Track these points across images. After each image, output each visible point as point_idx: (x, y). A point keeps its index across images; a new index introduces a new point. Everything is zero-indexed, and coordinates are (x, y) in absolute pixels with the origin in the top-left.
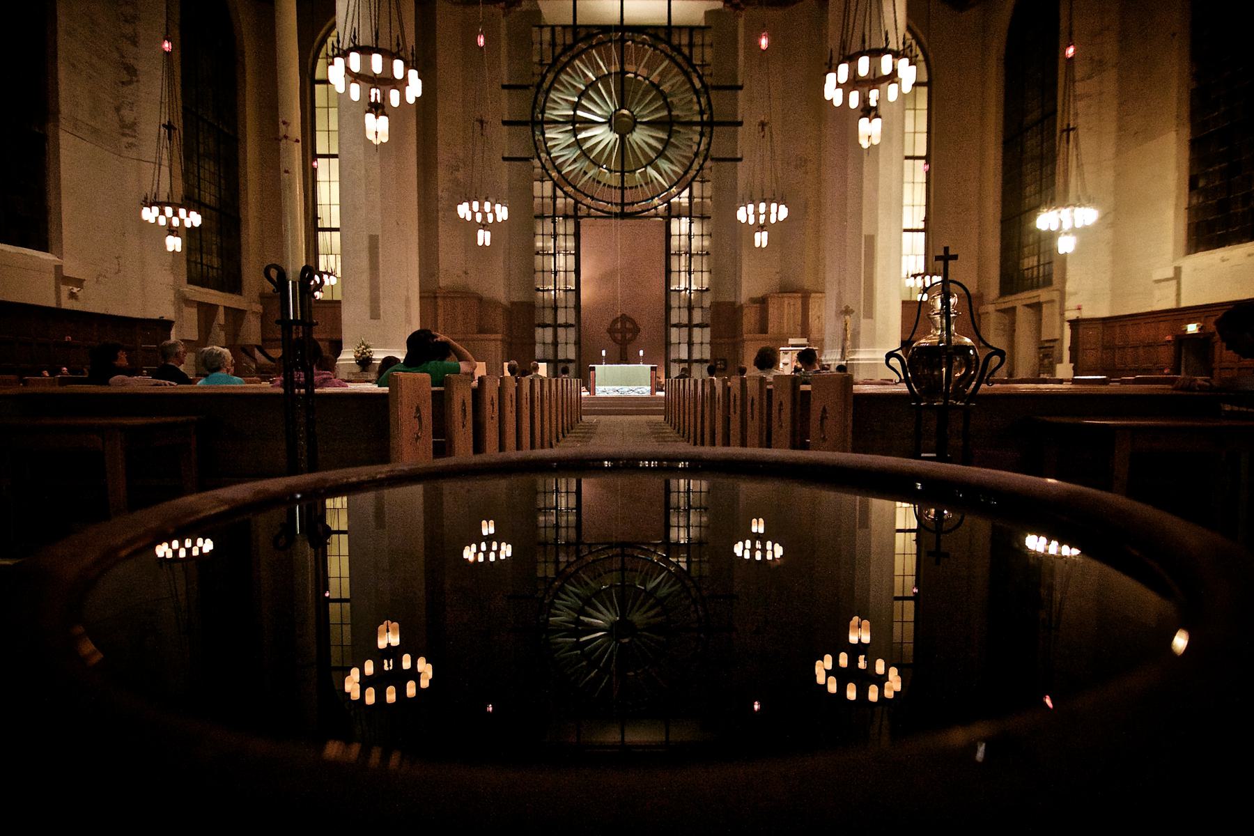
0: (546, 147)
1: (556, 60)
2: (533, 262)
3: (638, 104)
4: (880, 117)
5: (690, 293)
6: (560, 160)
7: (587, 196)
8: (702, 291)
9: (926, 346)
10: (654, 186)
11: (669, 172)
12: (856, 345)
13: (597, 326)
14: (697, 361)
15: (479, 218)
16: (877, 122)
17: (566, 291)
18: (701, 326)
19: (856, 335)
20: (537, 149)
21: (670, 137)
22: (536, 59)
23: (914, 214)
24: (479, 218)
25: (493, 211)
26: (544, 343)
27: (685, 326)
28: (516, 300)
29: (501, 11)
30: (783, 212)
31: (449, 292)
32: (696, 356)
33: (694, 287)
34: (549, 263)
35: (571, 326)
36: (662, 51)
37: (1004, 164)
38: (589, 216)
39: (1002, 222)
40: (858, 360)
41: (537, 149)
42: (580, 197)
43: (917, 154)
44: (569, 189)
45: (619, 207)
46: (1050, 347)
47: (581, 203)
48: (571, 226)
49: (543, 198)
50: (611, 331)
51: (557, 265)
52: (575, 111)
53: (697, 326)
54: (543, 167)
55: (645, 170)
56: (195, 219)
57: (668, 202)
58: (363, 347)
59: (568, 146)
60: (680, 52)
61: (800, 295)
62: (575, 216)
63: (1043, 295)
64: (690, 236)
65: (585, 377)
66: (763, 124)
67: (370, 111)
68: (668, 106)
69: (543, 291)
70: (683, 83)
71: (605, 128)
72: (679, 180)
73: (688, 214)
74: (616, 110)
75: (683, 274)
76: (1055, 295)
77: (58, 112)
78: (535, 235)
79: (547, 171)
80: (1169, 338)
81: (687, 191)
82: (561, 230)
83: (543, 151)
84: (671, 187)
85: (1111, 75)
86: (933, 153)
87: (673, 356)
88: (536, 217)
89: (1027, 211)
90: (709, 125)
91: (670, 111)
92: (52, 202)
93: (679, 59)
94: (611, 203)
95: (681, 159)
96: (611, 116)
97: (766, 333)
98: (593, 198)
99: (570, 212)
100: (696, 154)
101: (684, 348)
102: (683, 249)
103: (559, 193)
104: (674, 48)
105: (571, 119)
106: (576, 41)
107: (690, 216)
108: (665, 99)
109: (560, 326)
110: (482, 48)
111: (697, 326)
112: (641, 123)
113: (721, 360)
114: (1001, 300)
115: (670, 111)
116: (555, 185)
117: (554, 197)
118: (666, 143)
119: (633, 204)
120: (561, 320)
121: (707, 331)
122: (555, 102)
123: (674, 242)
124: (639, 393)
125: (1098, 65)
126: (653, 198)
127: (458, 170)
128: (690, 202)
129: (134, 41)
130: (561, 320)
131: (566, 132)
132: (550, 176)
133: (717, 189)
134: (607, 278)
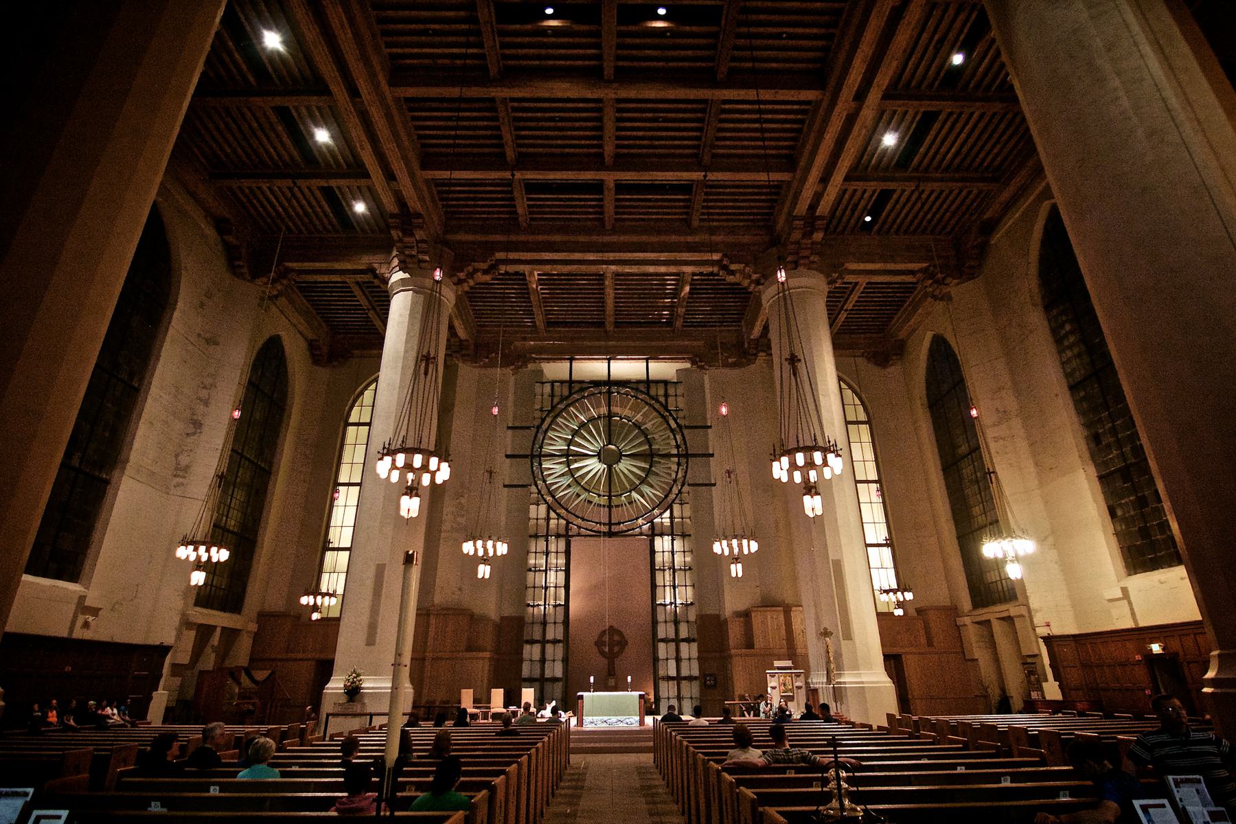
0: (542, 475)
1: (553, 407)
2: (525, 579)
3: (623, 440)
4: (819, 494)
5: (676, 607)
6: (553, 487)
7: (578, 517)
8: (687, 605)
10: (637, 506)
11: (651, 495)
12: (840, 668)
13: (585, 640)
14: (685, 678)
15: (481, 553)
16: (818, 498)
17: (555, 606)
18: (688, 640)
19: (838, 655)
20: (534, 478)
21: (651, 466)
22: (538, 407)
23: (877, 531)
24: (481, 553)
25: (494, 547)
26: (531, 660)
27: (672, 640)
28: (506, 615)
29: (511, 372)
30: (754, 546)
31: (443, 609)
32: (685, 673)
33: (678, 602)
34: (540, 579)
35: (559, 641)
36: (642, 400)
37: (948, 488)
38: (579, 535)
39: (958, 538)
40: (844, 683)
41: (534, 478)
42: (571, 518)
43: (870, 478)
44: (563, 512)
45: (607, 527)
46: (1032, 663)
47: (572, 523)
48: (562, 545)
49: (537, 519)
50: (599, 644)
51: (548, 581)
52: (569, 446)
53: (683, 640)
54: (539, 492)
55: (630, 495)
56: (222, 555)
57: (652, 522)
58: (354, 675)
59: (563, 475)
60: (657, 401)
61: (781, 608)
62: (566, 536)
63: (1013, 610)
64: (673, 553)
65: (571, 703)
66: (729, 472)
67: (406, 494)
68: (649, 442)
69: (533, 606)
70: (661, 425)
71: (595, 460)
72: (660, 503)
73: (670, 532)
74: (604, 445)
75: (668, 589)
76: (1023, 611)
77: (127, 461)
78: (528, 552)
79: (542, 496)
80: (1138, 657)
81: (668, 511)
82: (552, 548)
83: (540, 480)
84: (653, 509)
85: (1016, 423)
86: (883, 476)
87: (661, 673)
88: (531, 536)
89: (976, 530)
90: (685, 456)
91: (650, 446)
92: (96, 536)
93: (657, 406)
94: (600, 523)
95: (660, 484)
96: (600, 450)
97: (753, 648)
98: (583, 519)
99: (562, 531)
100: (675, 481)
101: (672, 664)
102: (666, 564)
103: (553, 515)
104: (652, 398)
105: (565, 452)
106: (571, 394)
107: (672, 534)
108: (646, 436)
109: (548, 642)
110: (495, 416)
111: (683, 640)
112: (625, 456)
113: (710, 675)
114: (974, 613)
115: (650, 446)
116: (549, 508)
117: (548, 519)
118: (648, 472)
119: (619, 523)
120: (550, 636)
121: (694, 646)
122: (551, 439)
123: (658, 558)
124: (627, 723)
125: (1004, 416)
126: (637, 519)
128: (672, 522)
129: (206, 403)
130: (550, 636)
131: (561, 463)
132: (545, 500)
133: (695, 510)
134: (593, 590)
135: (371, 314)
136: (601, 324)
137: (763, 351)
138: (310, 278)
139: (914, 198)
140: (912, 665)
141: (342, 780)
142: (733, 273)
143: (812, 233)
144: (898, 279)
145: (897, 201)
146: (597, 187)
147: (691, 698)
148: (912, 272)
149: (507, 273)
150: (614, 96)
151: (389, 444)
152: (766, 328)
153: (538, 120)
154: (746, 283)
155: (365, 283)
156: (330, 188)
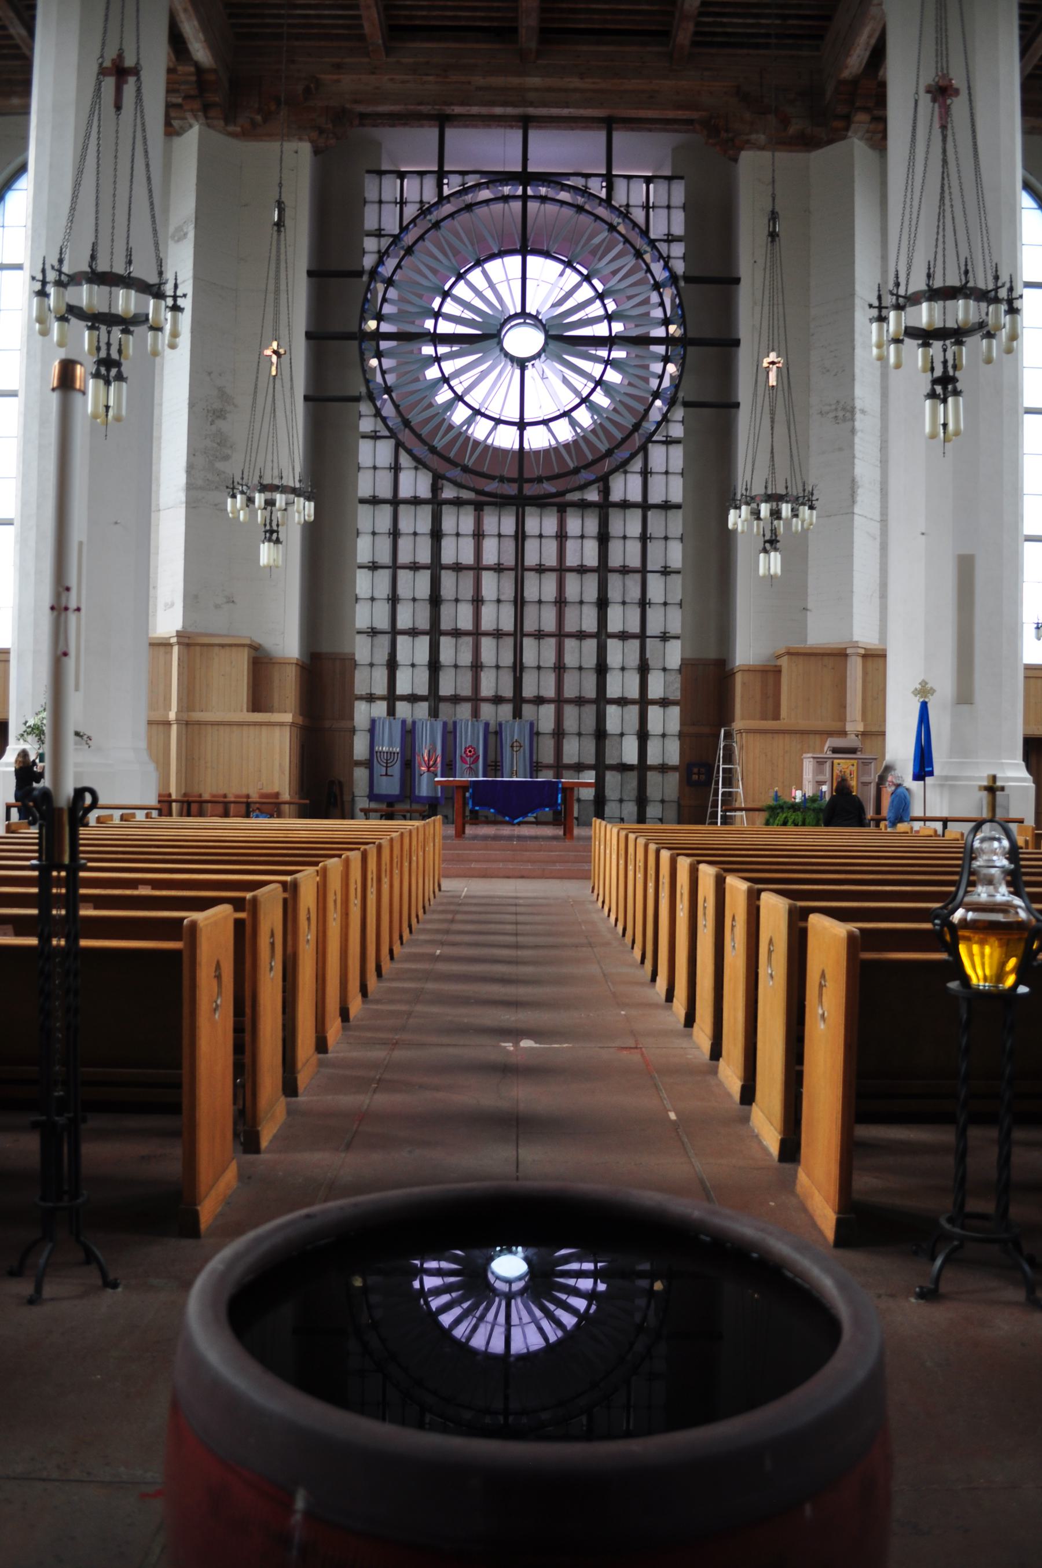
136: (506, 33)
137: (865, 109)
141: (35, 912)
152: (878, 54)
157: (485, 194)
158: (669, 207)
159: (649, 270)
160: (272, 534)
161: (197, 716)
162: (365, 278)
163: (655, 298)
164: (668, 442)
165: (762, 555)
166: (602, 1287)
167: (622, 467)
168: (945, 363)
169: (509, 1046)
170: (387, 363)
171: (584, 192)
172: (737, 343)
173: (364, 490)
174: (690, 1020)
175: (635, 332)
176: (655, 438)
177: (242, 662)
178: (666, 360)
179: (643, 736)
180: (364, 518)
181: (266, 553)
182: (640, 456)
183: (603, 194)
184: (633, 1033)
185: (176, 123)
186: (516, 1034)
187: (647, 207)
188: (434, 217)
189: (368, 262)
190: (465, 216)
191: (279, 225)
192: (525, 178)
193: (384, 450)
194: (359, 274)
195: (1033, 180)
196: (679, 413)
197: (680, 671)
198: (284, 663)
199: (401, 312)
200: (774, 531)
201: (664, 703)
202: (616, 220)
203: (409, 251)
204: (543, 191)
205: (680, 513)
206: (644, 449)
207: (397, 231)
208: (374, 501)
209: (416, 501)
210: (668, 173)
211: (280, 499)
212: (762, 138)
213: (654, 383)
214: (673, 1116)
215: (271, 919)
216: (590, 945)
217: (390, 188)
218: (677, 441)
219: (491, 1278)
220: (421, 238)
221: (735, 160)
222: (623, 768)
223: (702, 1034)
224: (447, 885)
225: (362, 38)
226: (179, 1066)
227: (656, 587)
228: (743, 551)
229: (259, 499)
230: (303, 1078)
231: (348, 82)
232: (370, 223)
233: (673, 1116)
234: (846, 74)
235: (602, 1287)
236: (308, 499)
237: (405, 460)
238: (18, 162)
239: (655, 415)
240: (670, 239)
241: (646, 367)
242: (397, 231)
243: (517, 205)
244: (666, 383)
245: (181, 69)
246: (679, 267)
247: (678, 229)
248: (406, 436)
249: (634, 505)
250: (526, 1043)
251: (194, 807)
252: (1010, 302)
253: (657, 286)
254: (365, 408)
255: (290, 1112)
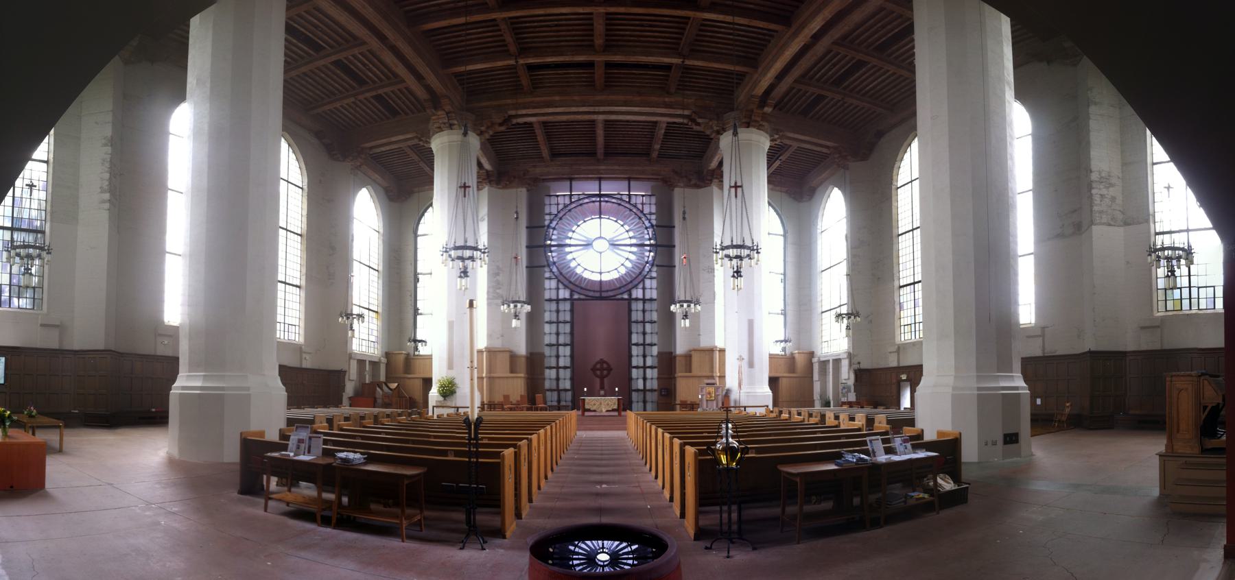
9: (924, 330)
18: (651, 367)
32: (648, 387)
53: (649, 367)
111: (649, 367)
121: (656, 370)
127: (498, 275)
135: (422, 165)
136: (593, 154)
137: (716, 178)
138: (378, 150)
139: (839, 104)
140: (784, 384)
142: (698, 124)
143: (763, 107)
144: (819, 149)
145: (827, 103)
146: (590, 65)
147: (652, 402)
148: (828, 147)
149: (518, 124)
150: (604, 11)
151: (446, 245)
152: (721, 164)
153: (536, 27)
154: (708, 132)
155: (413, 145)
156: (380, 95)
157: (586, 201)
158: (650, 204)
159: (644, 223)
160: (516, 316)
161: (493, 375)
162: (546, 228)
163: (646, 232)
164: (652, 278)
165: (683, 320)
166: (635, 562)
167: (636, 287)
168: (737, 266)
169: (599, 487)
170: (554, 254)
171: (621, 199)
172: (674, 246)
173: (547, 296)
174: (656, 477)
175: (639, 242)
176: (647, 277)
177: (507, 355)
178: (650, 251)
179: (645, 379)
180: (547, 306)
181: (514, 323)
182: (642, 283)
183: (627, 200)
184: (639, 482)
185: (480, 187)
186: (601, 483)
187: (643, 204)
188: (569, 208)
189: (547, 223)
190: (580, 208)
191: (517, 218)
192: (600, 196)
193: (553, 283)
194: (544, 226)
195: (770, 201)
196: (655, 269)
197: (657, 356)
198: (520, 357)
199: (558, 238)
200: (686, 312)
201: (651, 367)
202: (632, 208)
203: (561, 219)
204: (606, 199)
205: (656, 302)
206: (643, 280)
207: (556, 213)
208: (550, 300)
209: (565, 300)
210: (650, 194)
211: (519, 305)
212: (682, 185)
213: (646, 259)
214: (649, 507)
215: (524, 451)
216: (626, 453)
217: (554, 200)
218: (654, 278)
219: (597, 561)
220: (565, 215)
221: (673, 190)
222: (638, 390)
223: (660, 483)
224: (578, 433)
225: (542, 158)
226: (499, 494)
227: (648, 327)
228: (678, 317)
229: (512, 305)
230: (534, 498)
231: (538, 170)
232: (547, 211)
233: (649, 507)
234: (710, 168)
235: (635, 562)
236: (528, 304)
237: (561, 286)
238: (430, 202)
239: (647, 269)
240: (651, 214)
241: (643, 254)
242: (556, 213)
243: (598, 204)
244: (650, 259)
245: (481, 172)
246: (654, 222)
247: (654, 211)
248: (561, 278)
249: (640, 299)
250: (604, 486)
251: (492, 406)
252: (757, 249)
253: (646, 228)
254: (547, 269)
255: (530, 507)
